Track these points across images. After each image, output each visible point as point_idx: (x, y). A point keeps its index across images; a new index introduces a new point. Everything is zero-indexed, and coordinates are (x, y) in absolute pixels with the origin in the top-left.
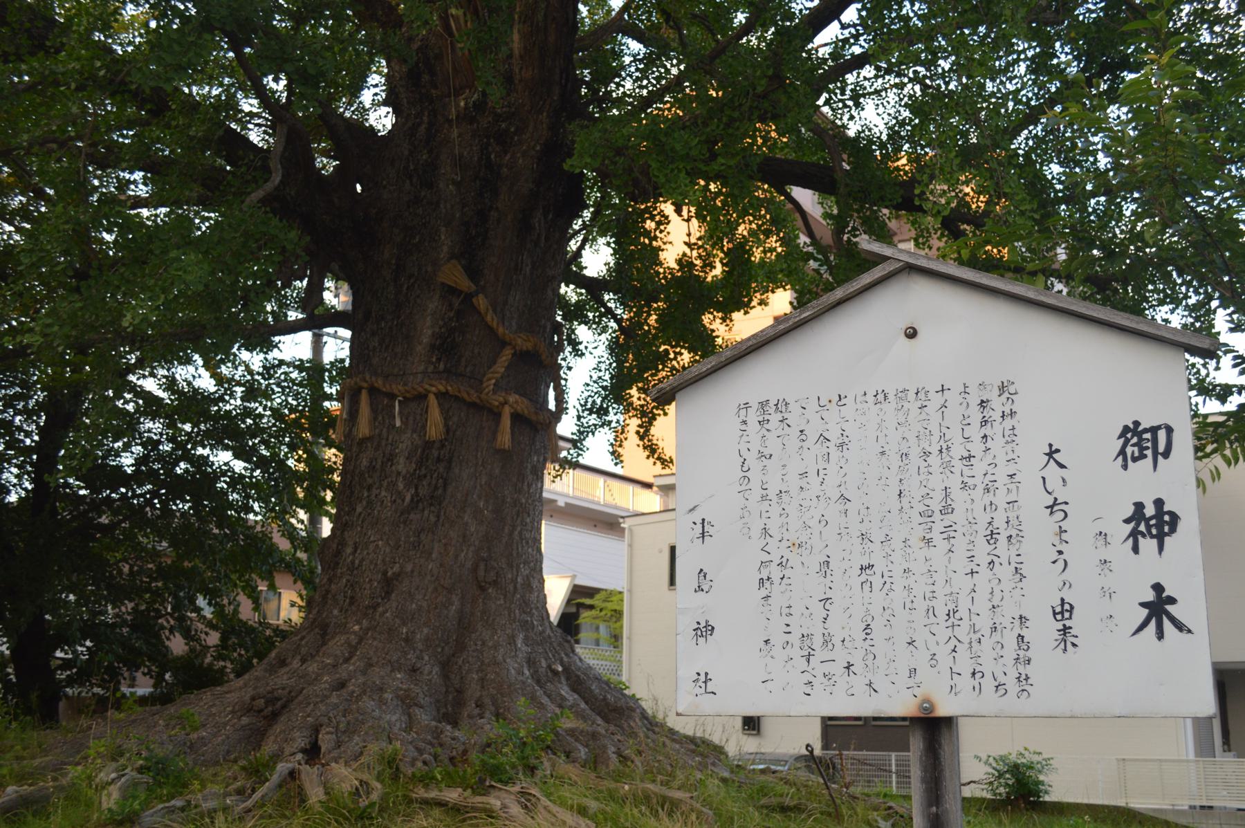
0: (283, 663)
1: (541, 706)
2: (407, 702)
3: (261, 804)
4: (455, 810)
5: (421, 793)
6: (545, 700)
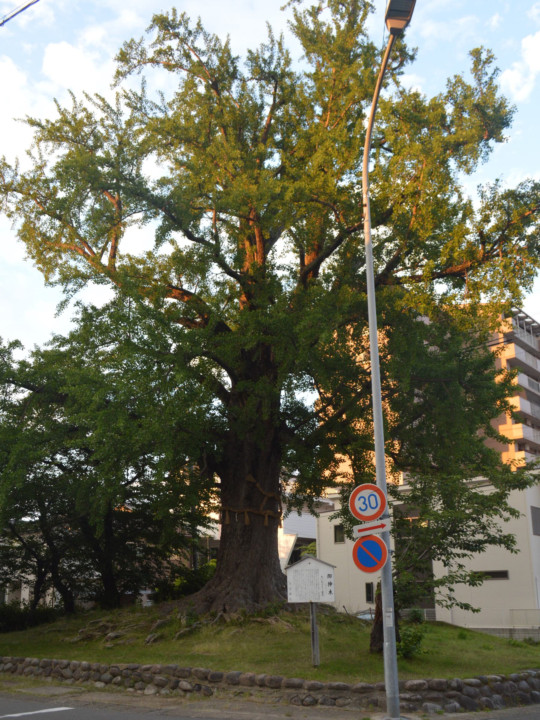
0: (210, 587)
1: (280, 598)
2: (245, 598)
3: (216, 622)
4: (260, 622)
5: (252, 619)
6: (281, 596)
